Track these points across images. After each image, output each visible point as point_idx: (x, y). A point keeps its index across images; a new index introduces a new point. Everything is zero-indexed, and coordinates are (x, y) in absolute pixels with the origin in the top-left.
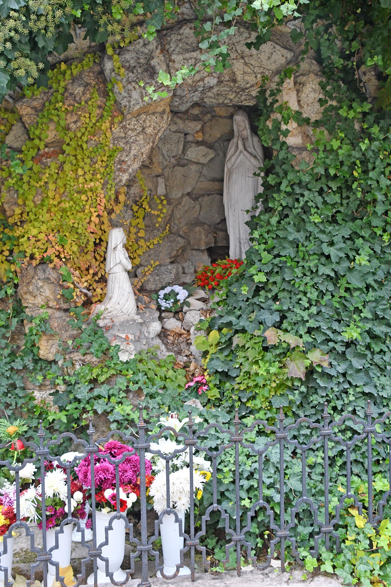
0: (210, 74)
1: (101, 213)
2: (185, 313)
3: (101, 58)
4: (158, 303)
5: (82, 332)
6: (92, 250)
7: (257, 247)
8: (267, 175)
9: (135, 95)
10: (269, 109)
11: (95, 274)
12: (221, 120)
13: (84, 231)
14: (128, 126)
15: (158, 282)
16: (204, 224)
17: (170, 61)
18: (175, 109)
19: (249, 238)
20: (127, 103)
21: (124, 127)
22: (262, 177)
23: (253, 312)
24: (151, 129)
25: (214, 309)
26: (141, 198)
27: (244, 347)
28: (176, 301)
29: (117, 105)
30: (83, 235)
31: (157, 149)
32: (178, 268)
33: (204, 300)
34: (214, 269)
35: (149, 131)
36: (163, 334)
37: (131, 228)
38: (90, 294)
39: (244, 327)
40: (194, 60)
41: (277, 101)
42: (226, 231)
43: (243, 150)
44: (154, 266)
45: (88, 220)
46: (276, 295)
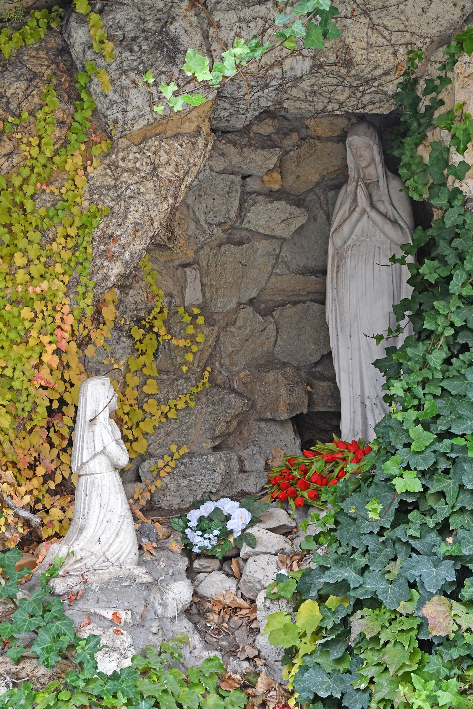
0: (295, 52)
1: (63, 344)
2: (246, 560)
3: (64, 20)
4: (185, 537)
5: (16, 607)
6: (44, 424)
7: (399, 417)
8: (420, 261)
9: (136, 98)
10: (422, 121)
11: (48, 477)
12: (319, 145)
13: (27, 384)
14: (121, 163)
15: (187, 492)
16: (285, 364)
17: (211, 24)
18: (222, 125)
19: (382, 394)
20: (120, 116)
21: (113, 166)
22: (410, 266)
23: (395, 559)
24: (171, 168)
25: (309, 552)
26: (149, 313)
27: (376, 639)
28: (226, 534)
29: (99, 120)
30: (25, 393)
31: (184, 209)
32: (229, 460)
33: (286, 532)
34: (308, 462)
35: (166, 172)
36: (196, 608)
37: (129, 375)
38: (36, 520)
39: (375, 593)
40: (260, 22)
41: (442, 103)
42: (333, 380)
43: (368, 209)
44: (176, 456)
45: (34, 362)
46: (446, 523)
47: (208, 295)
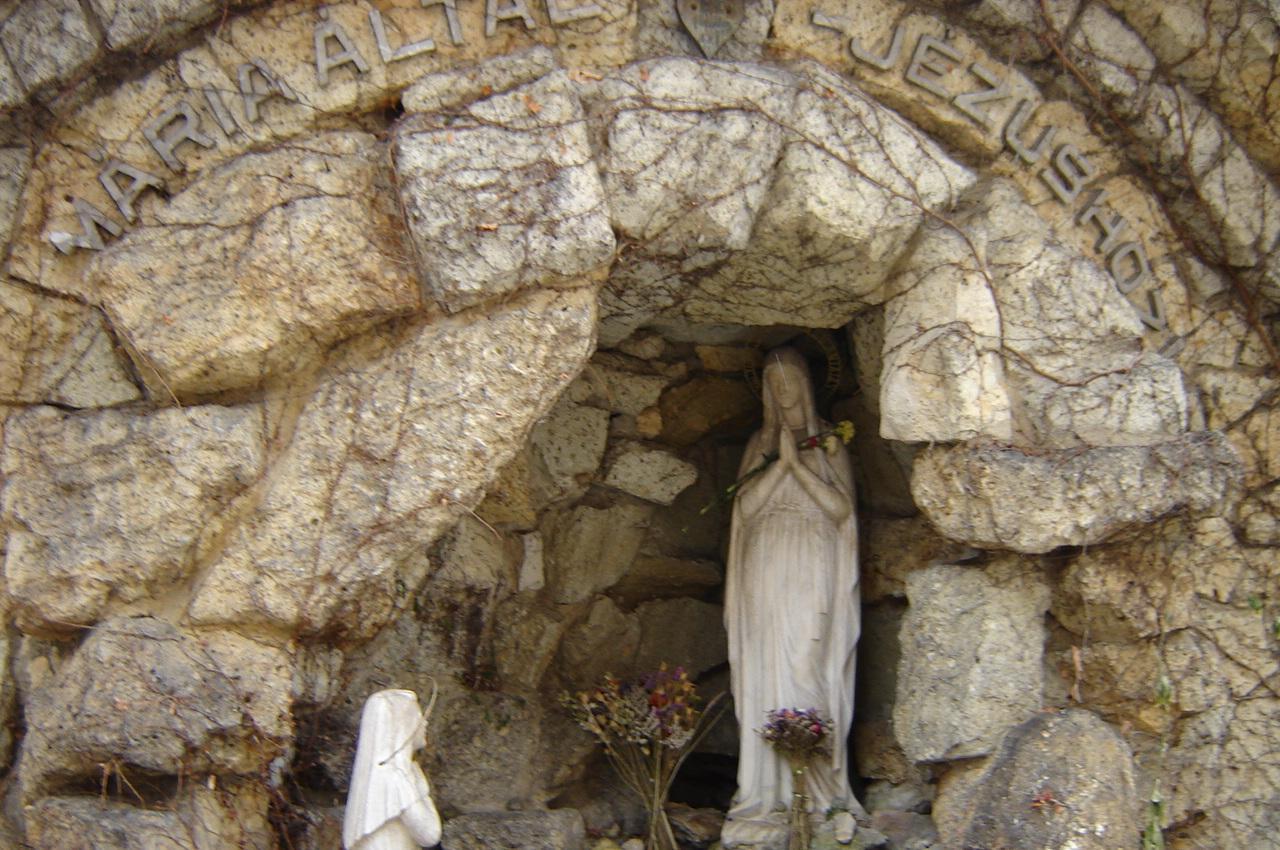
47: (550, 577)
